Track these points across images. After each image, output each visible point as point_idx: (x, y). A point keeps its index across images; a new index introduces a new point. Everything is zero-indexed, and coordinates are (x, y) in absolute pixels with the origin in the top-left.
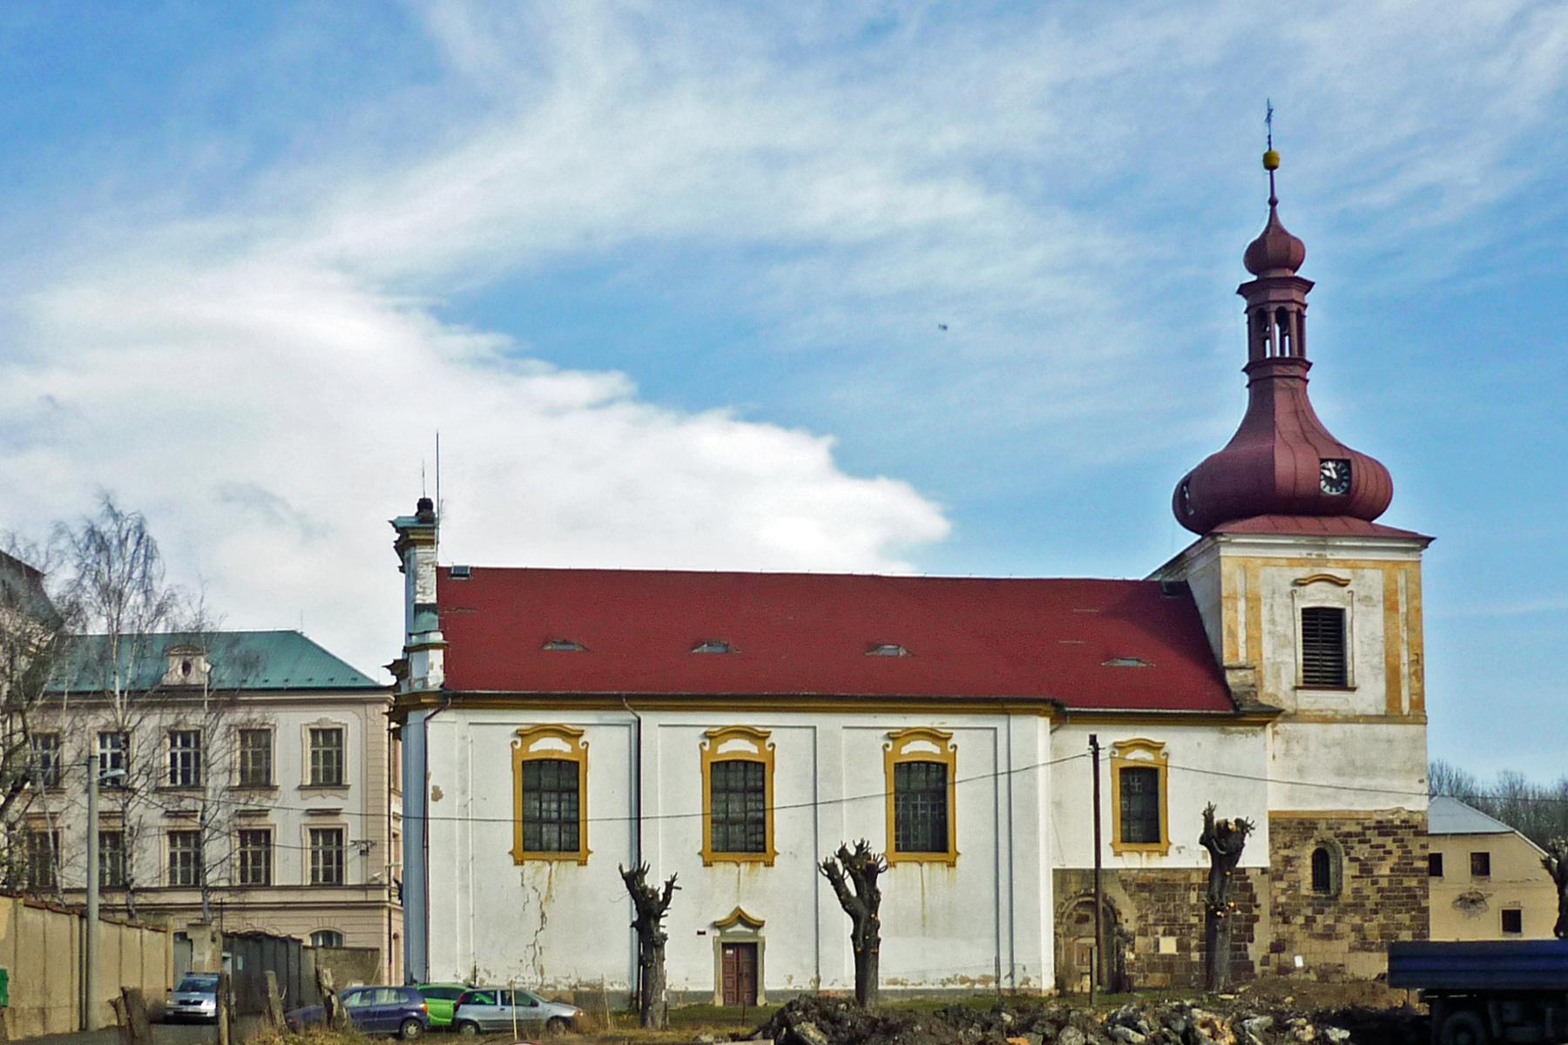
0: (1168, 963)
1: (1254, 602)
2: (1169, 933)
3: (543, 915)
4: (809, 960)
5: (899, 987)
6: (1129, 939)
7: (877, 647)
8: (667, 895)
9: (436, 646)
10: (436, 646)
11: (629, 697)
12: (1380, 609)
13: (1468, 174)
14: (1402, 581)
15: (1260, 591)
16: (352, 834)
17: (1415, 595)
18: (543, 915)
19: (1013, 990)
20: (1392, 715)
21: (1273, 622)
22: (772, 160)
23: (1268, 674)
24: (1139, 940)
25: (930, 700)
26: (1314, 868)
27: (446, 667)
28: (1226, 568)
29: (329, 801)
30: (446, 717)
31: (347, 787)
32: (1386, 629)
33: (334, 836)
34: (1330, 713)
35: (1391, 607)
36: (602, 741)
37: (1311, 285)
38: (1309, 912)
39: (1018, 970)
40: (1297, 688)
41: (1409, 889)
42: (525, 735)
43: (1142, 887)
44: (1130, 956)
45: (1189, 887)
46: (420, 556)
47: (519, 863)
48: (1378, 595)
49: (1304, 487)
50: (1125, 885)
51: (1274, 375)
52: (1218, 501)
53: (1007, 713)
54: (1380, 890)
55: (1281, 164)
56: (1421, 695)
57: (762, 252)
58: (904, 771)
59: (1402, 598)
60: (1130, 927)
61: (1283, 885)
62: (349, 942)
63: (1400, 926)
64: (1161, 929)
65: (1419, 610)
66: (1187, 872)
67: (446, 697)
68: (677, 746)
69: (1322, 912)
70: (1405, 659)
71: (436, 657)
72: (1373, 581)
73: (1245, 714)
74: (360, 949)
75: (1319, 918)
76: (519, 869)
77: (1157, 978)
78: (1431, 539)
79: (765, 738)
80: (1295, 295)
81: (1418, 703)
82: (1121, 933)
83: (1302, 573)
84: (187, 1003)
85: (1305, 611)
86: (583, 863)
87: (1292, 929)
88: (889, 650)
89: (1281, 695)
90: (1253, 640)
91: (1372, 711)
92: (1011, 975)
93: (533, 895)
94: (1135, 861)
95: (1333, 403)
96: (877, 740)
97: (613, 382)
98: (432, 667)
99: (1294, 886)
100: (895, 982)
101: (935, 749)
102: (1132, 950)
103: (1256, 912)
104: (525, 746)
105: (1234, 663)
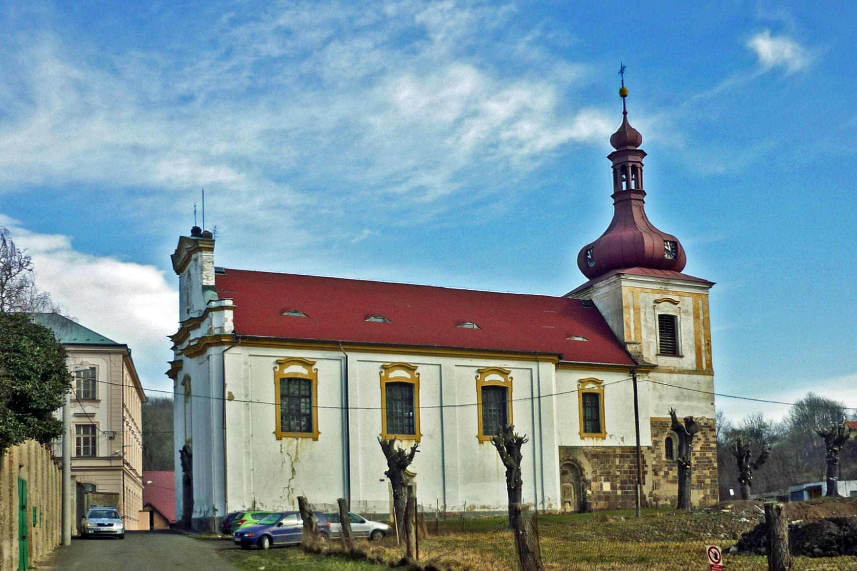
0: (607, 497)
1: (637, 310)
2: (607, 480)
3: (293, 470)
4: (440, 495)
5: (486, 510)
6: (588, 483)
7: (463, 323)
8: (411, 456)
9: (228, 308)
10: (228, 308)
11: (343, 343)
12: (692, 317)
13: (437, 183)
14: (701, 304)
15: (638, 302)
16: (103, 427)
17: (707, 311)
18: (293, 470)
19: (544, 511)
20: (698, 371)
21: (646, 321)
22: (138, 150)
23: (644, 346)
24: (593, 484)
25: (501, 352)
26: (667, 448)
27: (235, 321)
28: (625, 291)
29: (89, 408)
30: (236, 350)
31: (99, 401)
32: (695, 327)
33: (93, 428)
34: (672, 368)
35: (697, 317)
36: (326, 367)
37: (645, 155)
38: (666, 469)
39: (546, 499)
40: (657, 355)
41: (708, 458)
42: (282, 363)
43: (595, 456)
44: (589, 492)
45: (615, 456)
46: (204, 257)
47: (279, 439)
48: (691, 310)
49: (658, 253)
50: (586, 455)
51: (627, 199)
52: (601, 263)
53: (537, 360)
54: (696, 458)
55: (628, 94)
56: (711, 361)
57: (133, 192)
58: (486, 390)
59: (701, 312)
60: (589, 477)
61: (654, 455)
62: (100, 489)
63: (705, 477)
64: (603, 478)
65: (708, 318)
66: (614, 448)
67: (237, 338)
68: (368, 371)
69: (671, 469)
70: (703, 342)
71: (229, 315)
72: (688, 303)
73: (640, 367)
74: (109, 494)
75: (671, 472)
76: (279, 442)
77: (602, 504)
78: (713, 284)
79: (414, 370)
80: (639, 159)
81: (710, 365)
82: (584, 480)
83: (658, 297)
84: (103, 525)
85: (661, 317)
86: (316, 439)
87: (659, 477)
88: (468, 325)
89: (651, 358)
90: (638, 329)
91: (690, 368)
92: (543, 502)
93: (287, 458)
94: (590, 442)
95: (658, 215)
96: (472, 373)
97: (59, 241)
98: (226, 320)
99: (659, 456)
100: (484, 507)
101: (502, 380)
102: (590, 489)
103: (646, 469)
104: (281, 369)
105: (629, 341)
